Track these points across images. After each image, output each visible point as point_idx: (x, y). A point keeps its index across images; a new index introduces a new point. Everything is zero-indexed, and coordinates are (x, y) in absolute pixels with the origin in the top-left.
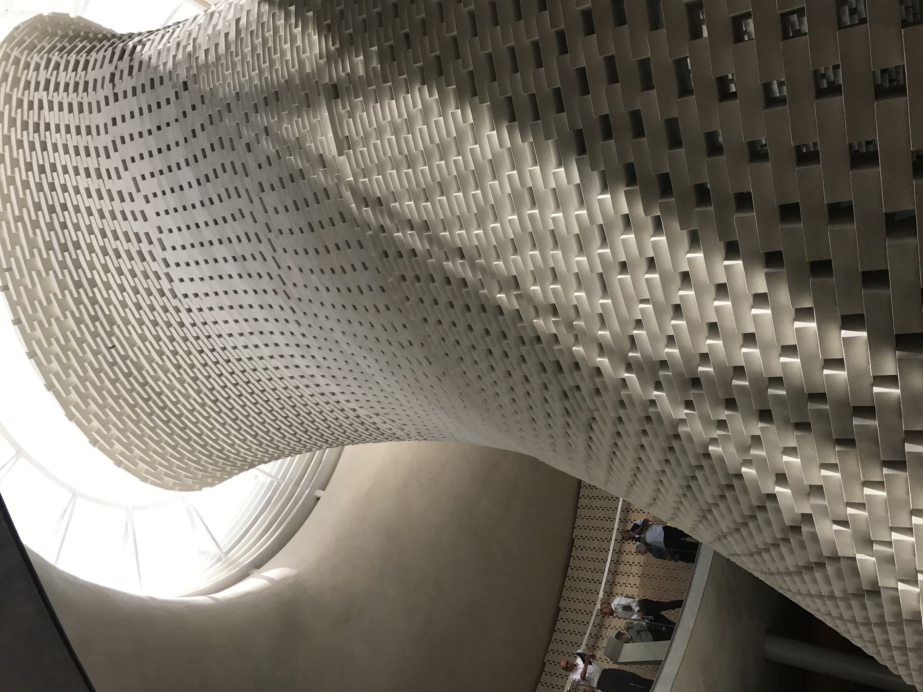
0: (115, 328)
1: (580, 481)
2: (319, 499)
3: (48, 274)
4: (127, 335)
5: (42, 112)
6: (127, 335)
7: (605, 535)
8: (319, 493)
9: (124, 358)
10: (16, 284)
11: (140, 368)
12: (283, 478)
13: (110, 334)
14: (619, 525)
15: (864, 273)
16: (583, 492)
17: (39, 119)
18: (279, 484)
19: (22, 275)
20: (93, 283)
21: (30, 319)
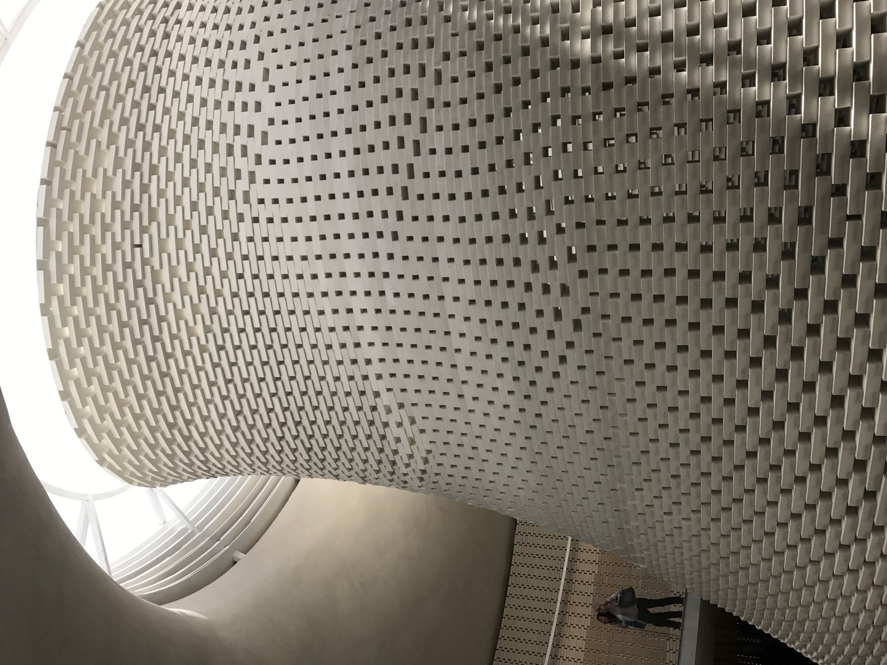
0: (154, 224)
1: (514, 522)
2: (235, 563)
3: (108, 148)
4: (163, 235)
5: (177, 11)
6: (163, 235)
7: (557, 553)
8: (239, 555)
9: (145, 262)
10: (68, 145)
11: (156, 280)
12: (200, 528)
13: (143, 230)
14: (566, 544)
15: (690, 323)
16: (519, 528)
17: (172, 15)
18: (192, 534)
19: (79, 138)
20: (154, 170)
21: (63, 185)
